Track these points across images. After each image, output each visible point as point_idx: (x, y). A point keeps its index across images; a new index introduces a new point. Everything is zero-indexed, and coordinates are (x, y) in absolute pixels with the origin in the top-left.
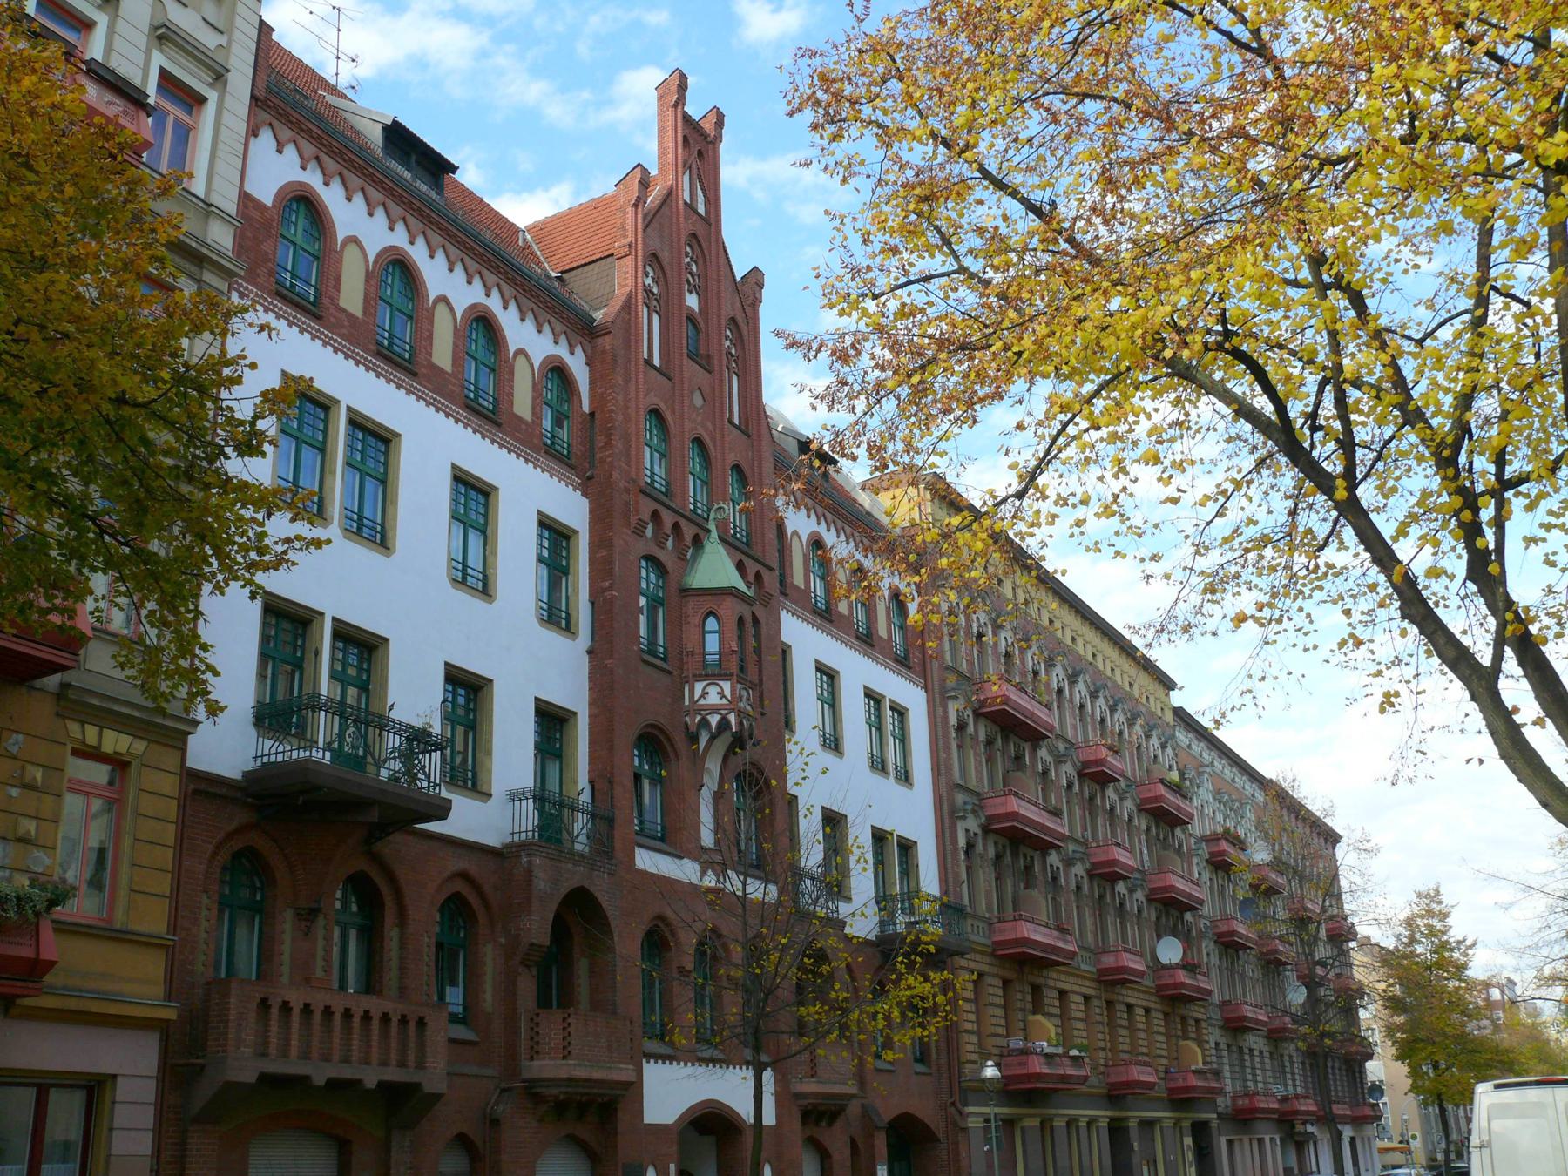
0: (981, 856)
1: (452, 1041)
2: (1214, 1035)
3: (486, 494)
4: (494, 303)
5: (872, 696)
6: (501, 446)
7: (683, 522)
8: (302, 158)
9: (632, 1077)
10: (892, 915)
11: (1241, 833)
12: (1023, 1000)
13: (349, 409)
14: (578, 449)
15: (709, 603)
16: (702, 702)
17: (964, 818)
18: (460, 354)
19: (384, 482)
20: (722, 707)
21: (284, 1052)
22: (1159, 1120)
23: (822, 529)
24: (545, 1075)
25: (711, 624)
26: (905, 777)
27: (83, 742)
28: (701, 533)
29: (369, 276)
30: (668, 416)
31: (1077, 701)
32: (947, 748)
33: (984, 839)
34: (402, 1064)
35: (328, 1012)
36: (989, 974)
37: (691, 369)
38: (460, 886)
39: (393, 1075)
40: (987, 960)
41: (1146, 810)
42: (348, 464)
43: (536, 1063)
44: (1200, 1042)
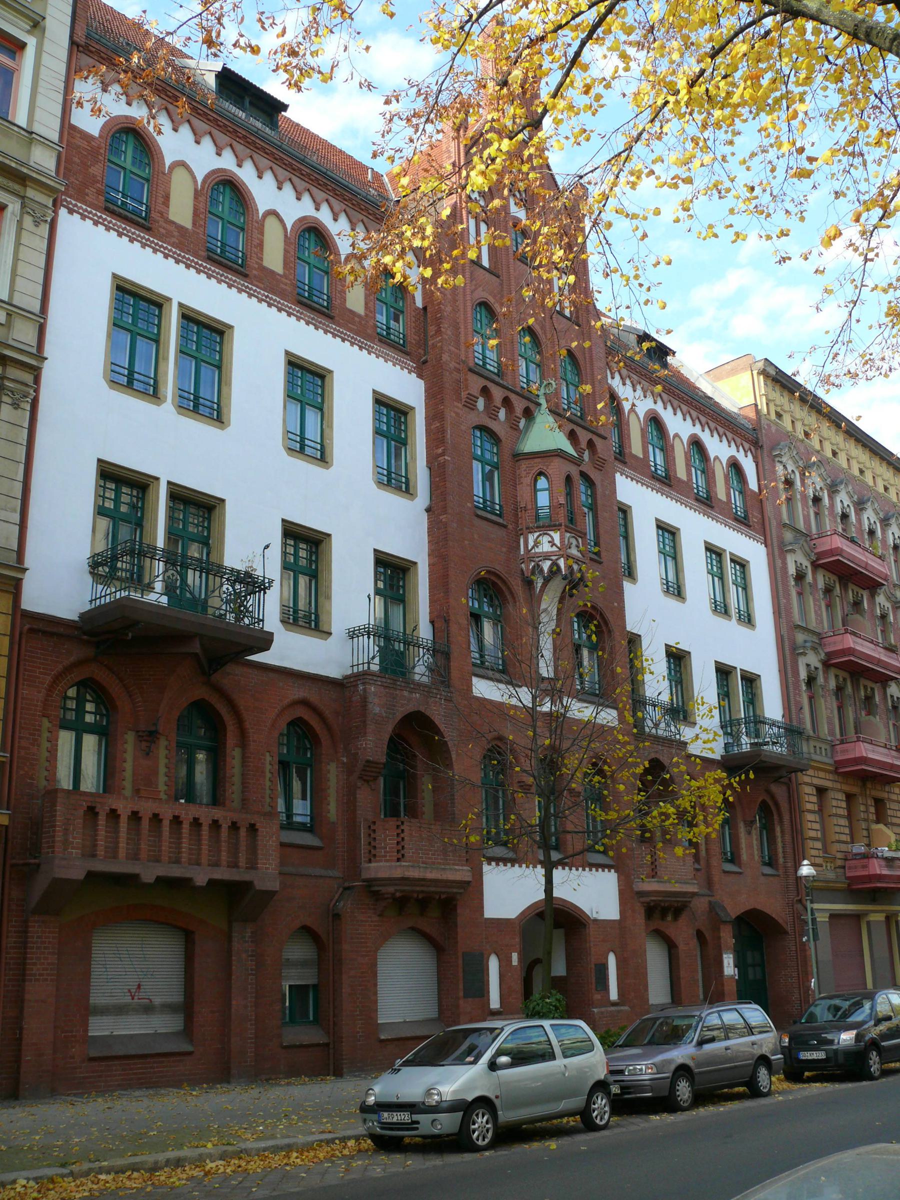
0: (823, 688)
1: (283, 845)
3: (322, 377)
4: (324, 216)
5: (710, 549)
6: (334, 336)
7: (513, 397)
8: (195, 134)
9: (468, 877)
10: (737, 738)
12: (867, 811)
13: (181, 305)
14: (413, 338)
15: (538, 465)
17: (804, 654)
18: (292, 258)
19: (219, 367)
20: (552, 554)
21: (113, 853)
24: (381, 875)
25: (542, 483)
26: (747, 619)
28: (532, 406)
29: (197, 194)
31: (810, 492)
32: (788, 596)
33: (826, 672)
34: (234, 865)
35: (156, 818)
36: (832, 789)
40: (831, 777)
42: (114, 325)
43: (373, 865)
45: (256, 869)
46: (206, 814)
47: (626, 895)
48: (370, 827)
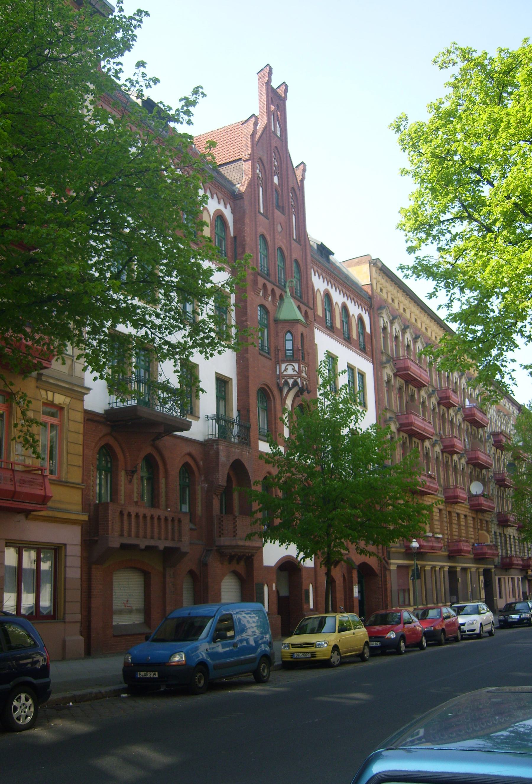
2: (494, 528)
7: (276, 289)
11: (508, 431)
16: (285, 373)
20: (294, 375)
22: (470, 568)
23: (329, 287)
27: (47, 399)
28: (283, 293)
30: (268, 238)
34: (173, 539)
36: (469, 516)
37: (277, 213)
38: (188, 459)
39: (169, 544)
41: (467, 421)
43: (222, 538)
44: (488, 531)
45: (181, 541)
46: (149, 512)
48: (220, 519)
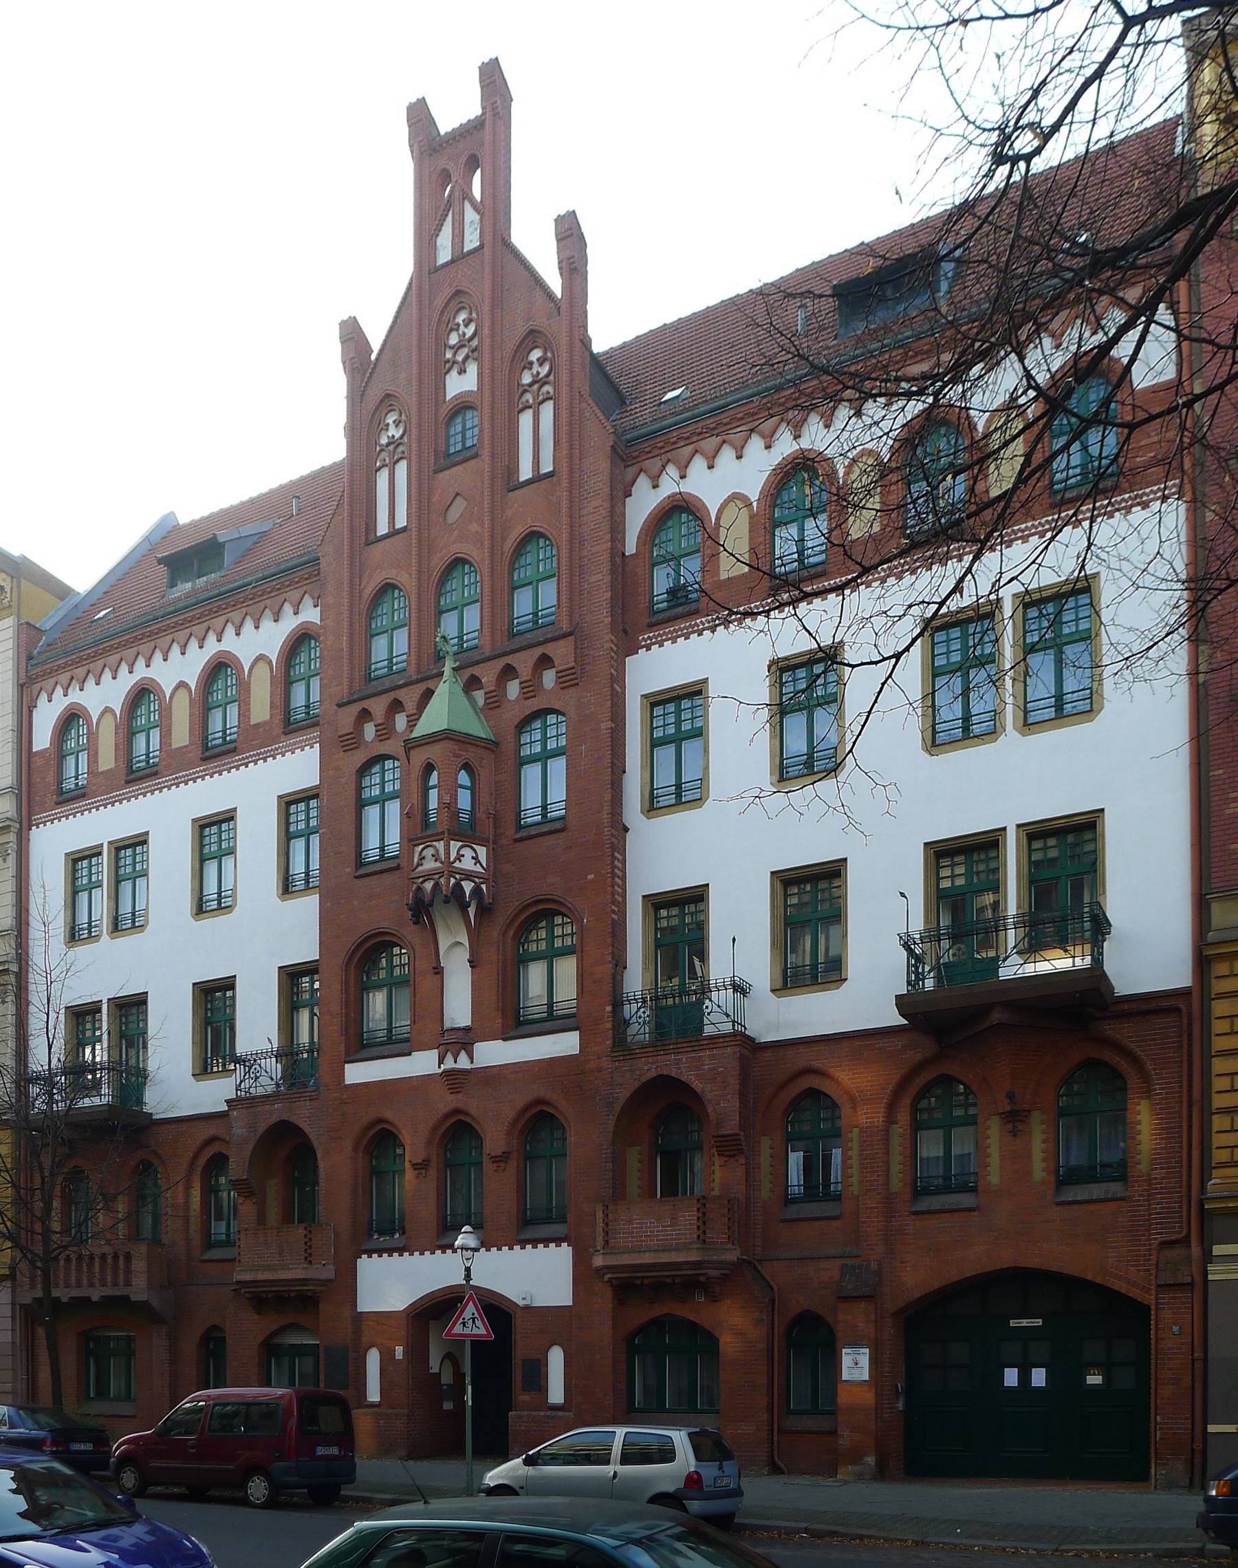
34: (115, 1284)
47: (582, 1275)
